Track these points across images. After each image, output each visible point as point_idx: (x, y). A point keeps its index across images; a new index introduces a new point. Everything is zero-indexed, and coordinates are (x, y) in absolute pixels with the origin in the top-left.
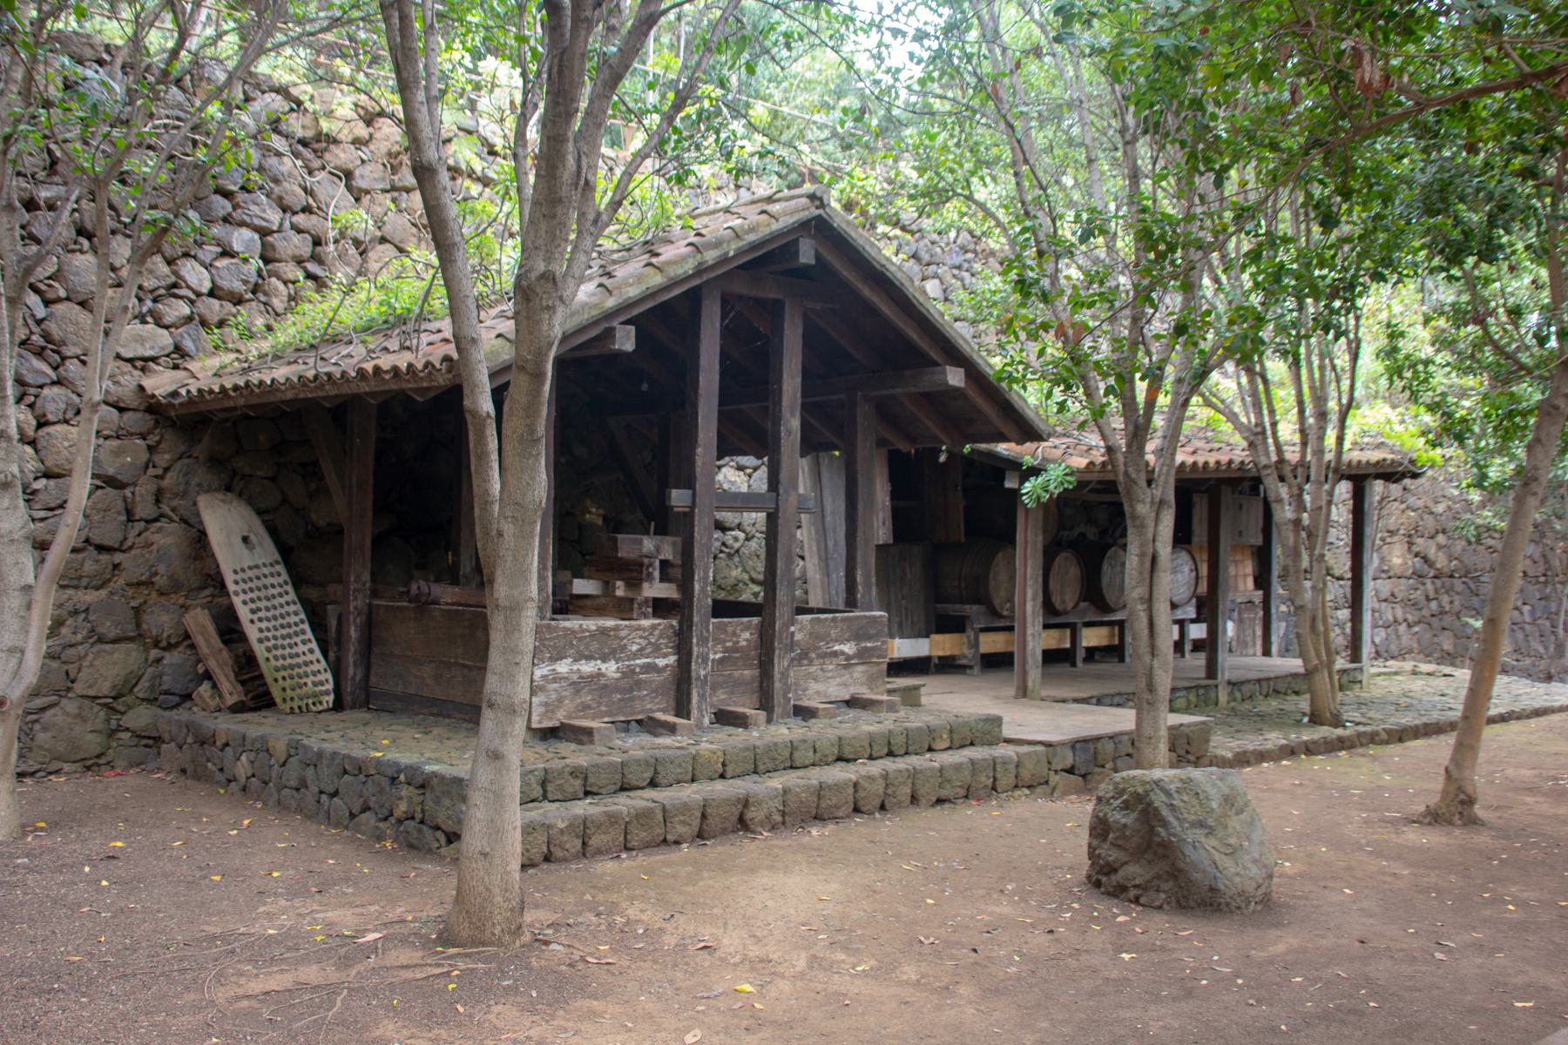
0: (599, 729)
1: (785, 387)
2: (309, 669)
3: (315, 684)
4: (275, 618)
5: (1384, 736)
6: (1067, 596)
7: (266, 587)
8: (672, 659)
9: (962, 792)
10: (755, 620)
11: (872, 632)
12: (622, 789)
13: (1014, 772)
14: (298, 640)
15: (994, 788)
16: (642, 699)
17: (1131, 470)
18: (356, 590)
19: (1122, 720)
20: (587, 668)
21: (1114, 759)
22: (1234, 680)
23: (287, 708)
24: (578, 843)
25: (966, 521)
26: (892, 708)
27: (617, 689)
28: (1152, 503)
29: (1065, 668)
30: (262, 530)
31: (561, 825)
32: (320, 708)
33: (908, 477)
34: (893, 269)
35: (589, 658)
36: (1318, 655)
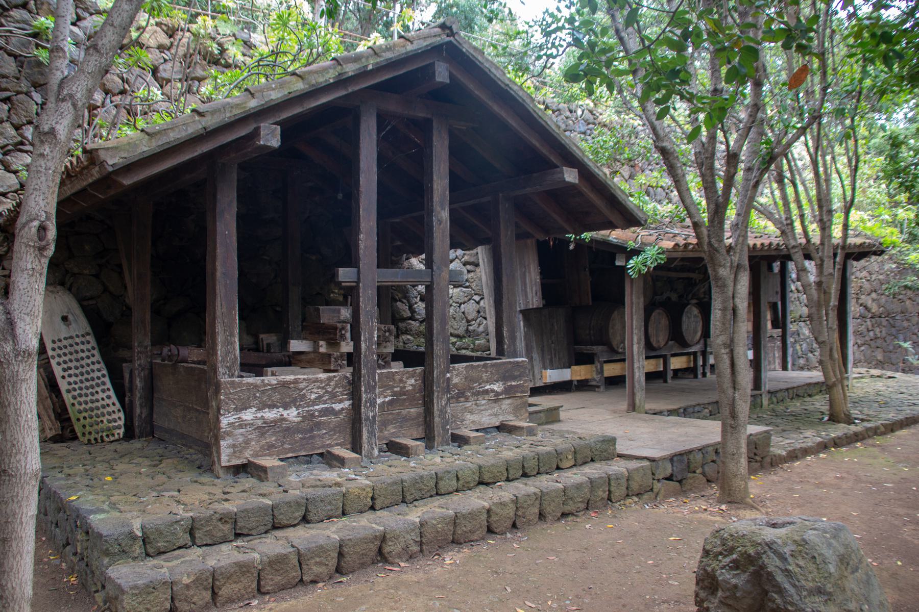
0: (273, 468)
1: (435, 186)
2: (105, 411)
3: (109, 421)
4: (82, 374)
5: (882, 429)
6: (660, 338)
7: (77, 352)
8: (347, 404)
9: (583, 506)
10: (419, 369)
11: (516, 373)
12: (275, 527)
13: (625, 484)
14: (99, 389)
15: (609, 499)
16: (322, 436)
17: (713, 240)
18: (139, 352)
19: (706, 432)
20: (270, 415)
21: (703, 466)
22: (772, 390)
23: (85, 440)
24: (207, 595)
25: (596, 297)
26: (531, 432)
27: (298, 431)
28: (731, 267)
29: (659, 384)
30: (78, 311)
31: (186, 580)
32: (112, 439)
33: (555, 263)
34: (515, 88)
35: (272, 406)
36: (835, 375)
